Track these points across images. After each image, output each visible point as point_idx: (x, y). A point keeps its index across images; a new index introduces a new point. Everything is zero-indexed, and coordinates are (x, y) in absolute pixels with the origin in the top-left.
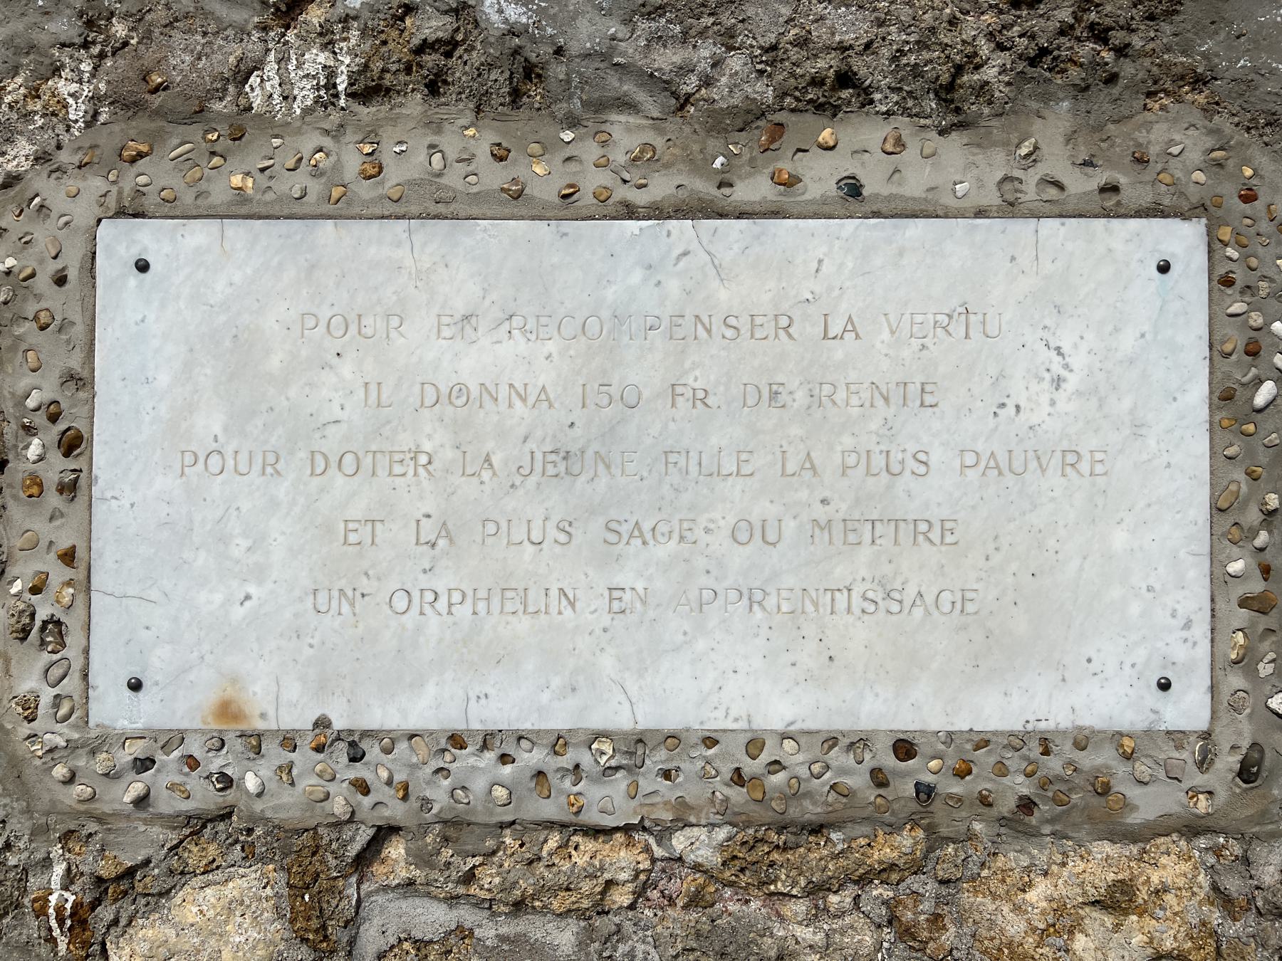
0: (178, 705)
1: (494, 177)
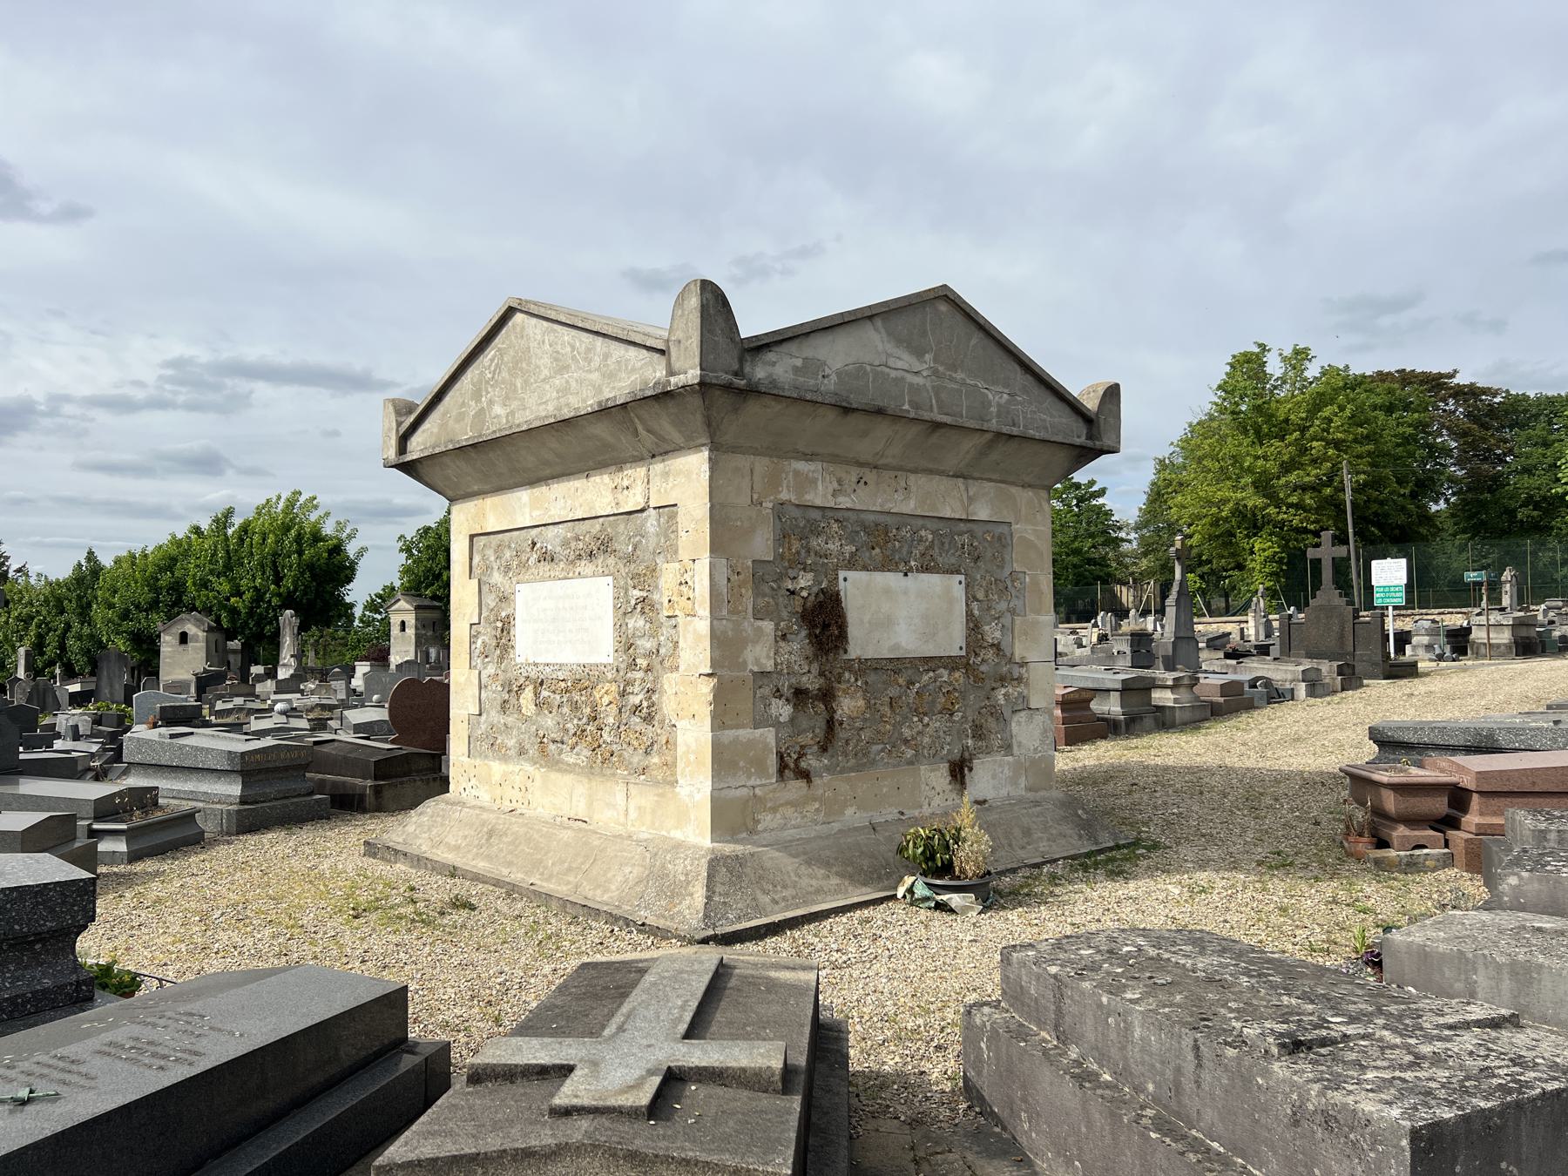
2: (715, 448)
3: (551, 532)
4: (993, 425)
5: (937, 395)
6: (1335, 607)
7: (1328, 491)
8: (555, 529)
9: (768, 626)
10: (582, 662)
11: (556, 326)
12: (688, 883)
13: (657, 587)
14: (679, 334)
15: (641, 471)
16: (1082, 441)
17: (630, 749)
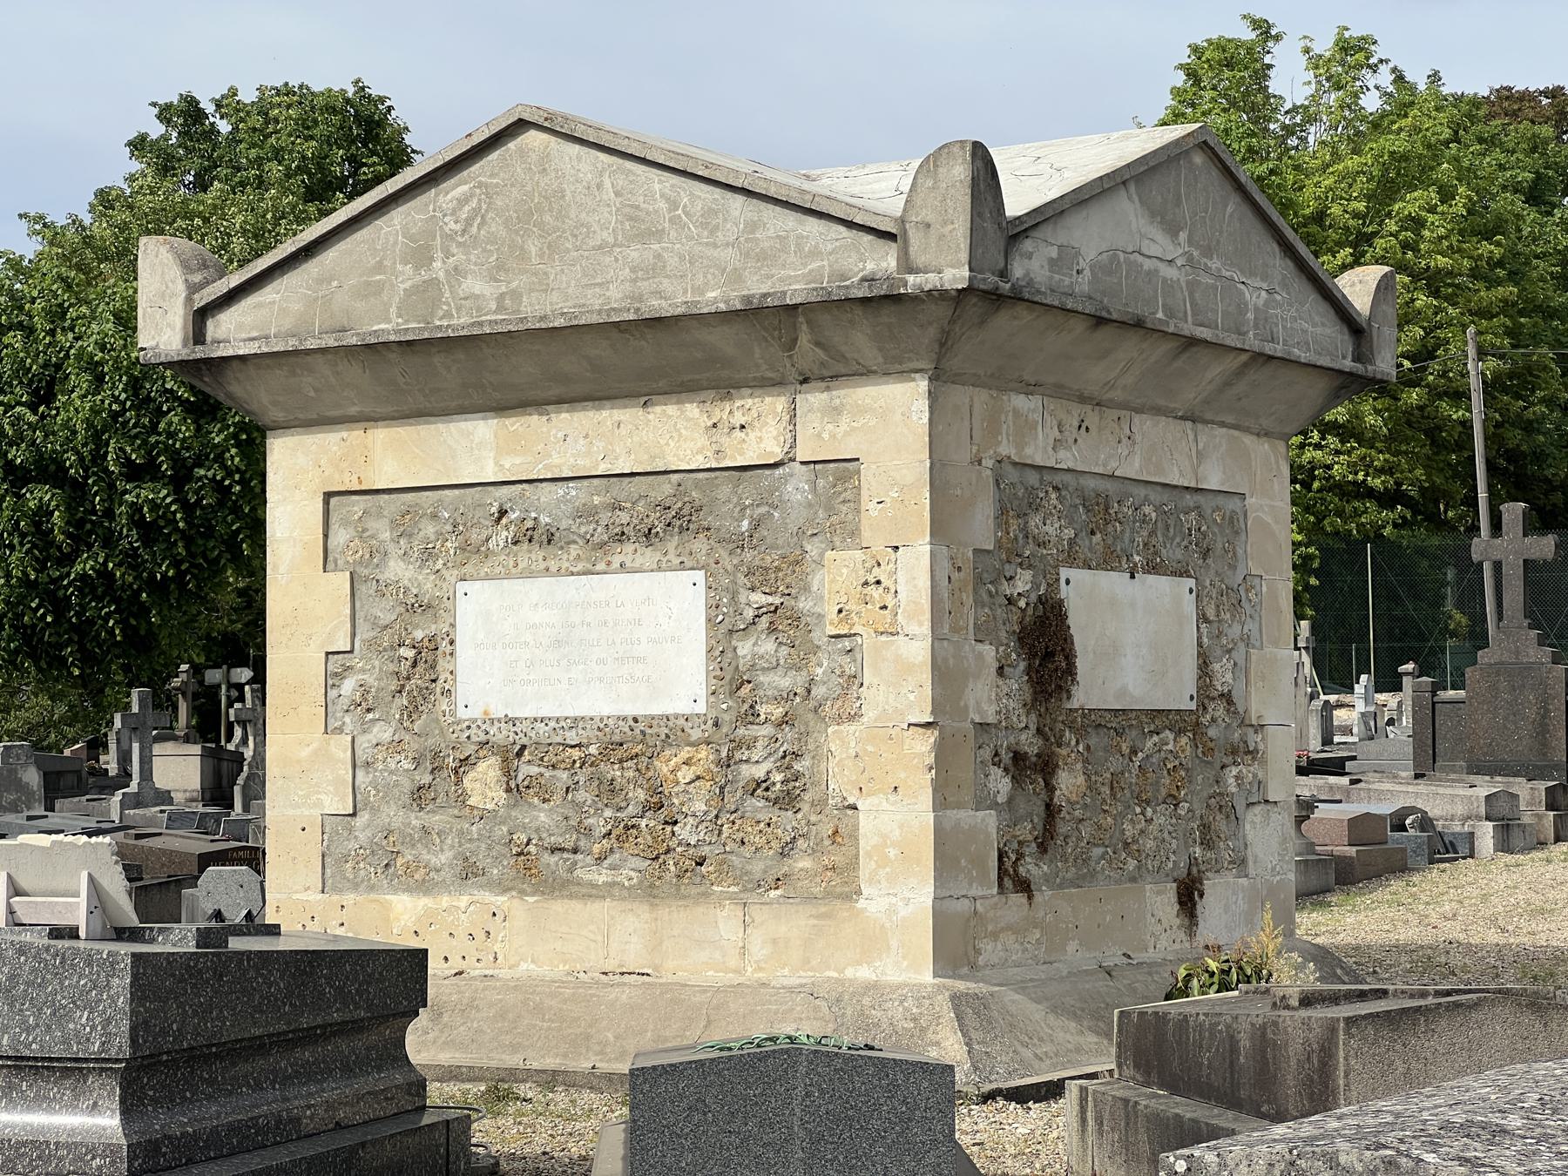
0: (475, 712)
1: (542, 565)
2: (938, 377)
3: (548, 493)
4: (1252, 342)
5: (1191, 294)
6: (1529, 667)
7: (1414, 396)
8: (560, 490)
9: (989, 652)
10: (630, 711)
11: (629, 165)
12: (923, 1030)
13: (806, 589)
14: (927, 215)
15: (776, 404)
16: (1348, 364)
17: (747, 851)
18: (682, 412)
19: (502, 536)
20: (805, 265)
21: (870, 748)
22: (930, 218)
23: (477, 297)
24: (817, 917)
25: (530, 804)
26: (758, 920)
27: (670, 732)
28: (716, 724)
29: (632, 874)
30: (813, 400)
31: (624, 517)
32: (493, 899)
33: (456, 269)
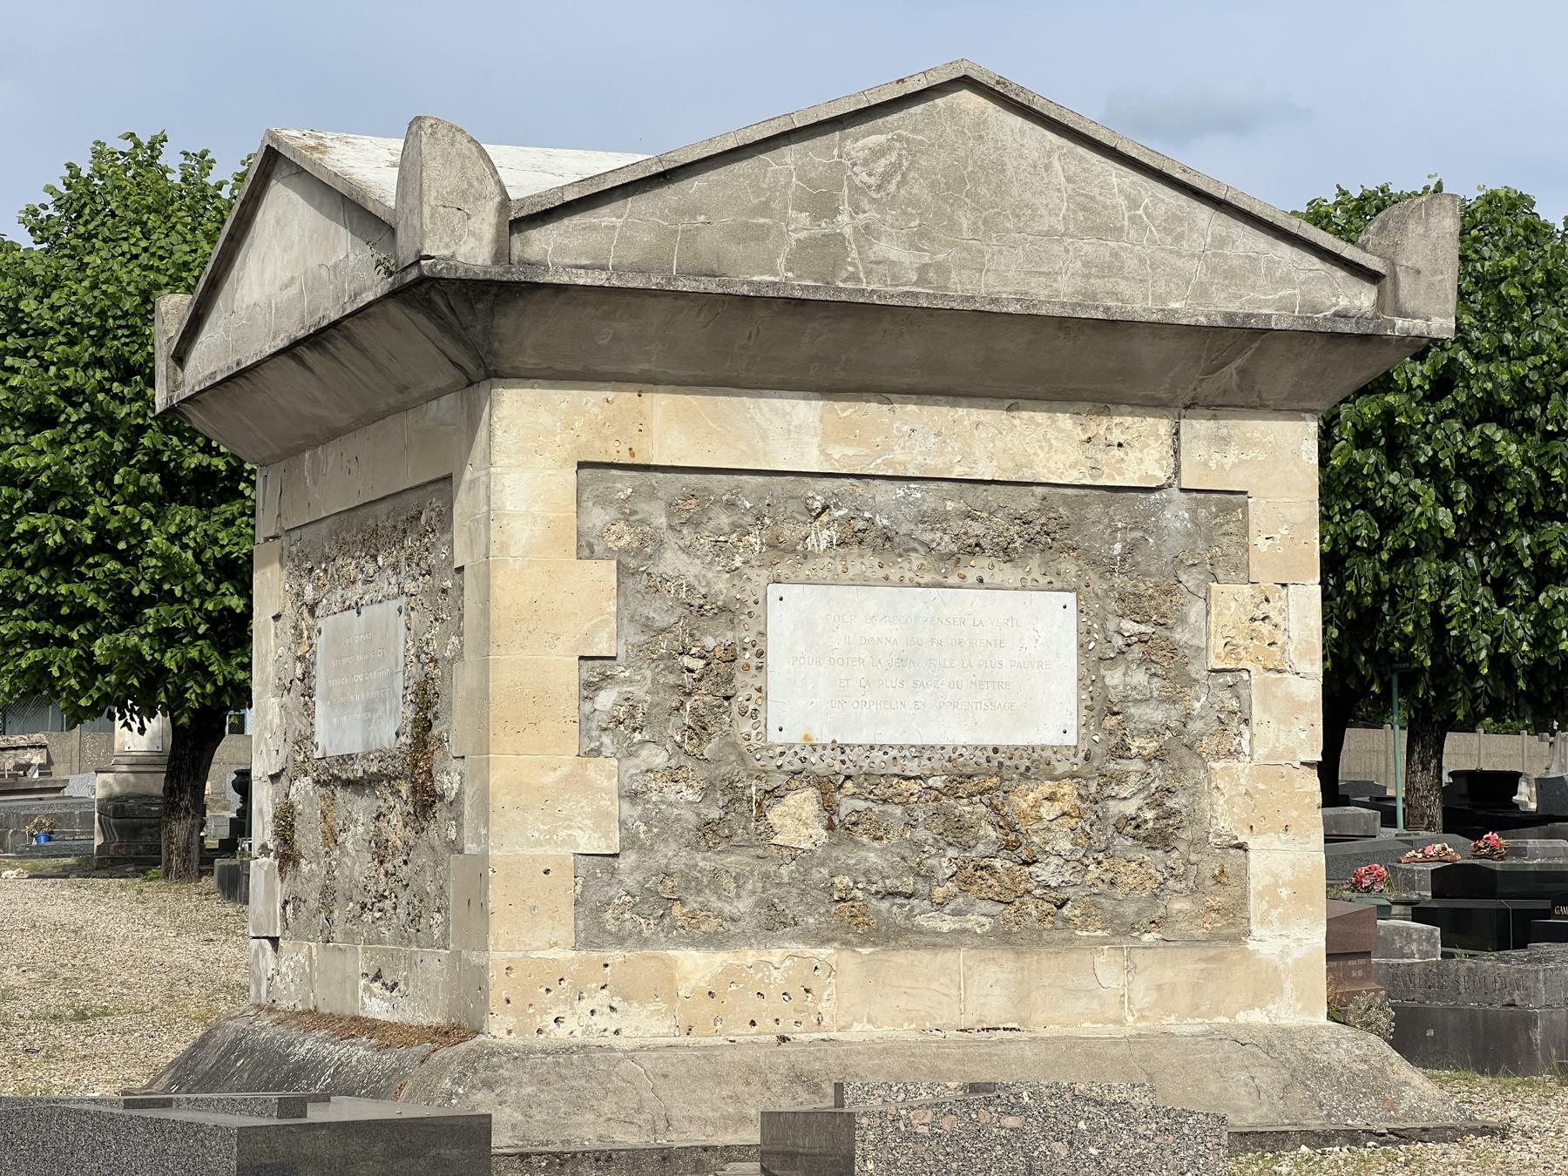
0: (793, 736)
1: (881, 573)
3: (884, 493)
8: (899, 490)
10: (990, 740)
18: (1054, 422)
19: (821, 537)
20: (1276, 291)
21: (1261, 786)
22: (1420, 265)
23: (893, 263)
24: (1208, 960)
25: (856, 843)
26: (1140, 966)
27: (1035, 765)
28: (1086, 758)
29: (984, 919)
30: (1197, 428)
31: (977, 528)
32: (816, 951)
33: (867, 227)
